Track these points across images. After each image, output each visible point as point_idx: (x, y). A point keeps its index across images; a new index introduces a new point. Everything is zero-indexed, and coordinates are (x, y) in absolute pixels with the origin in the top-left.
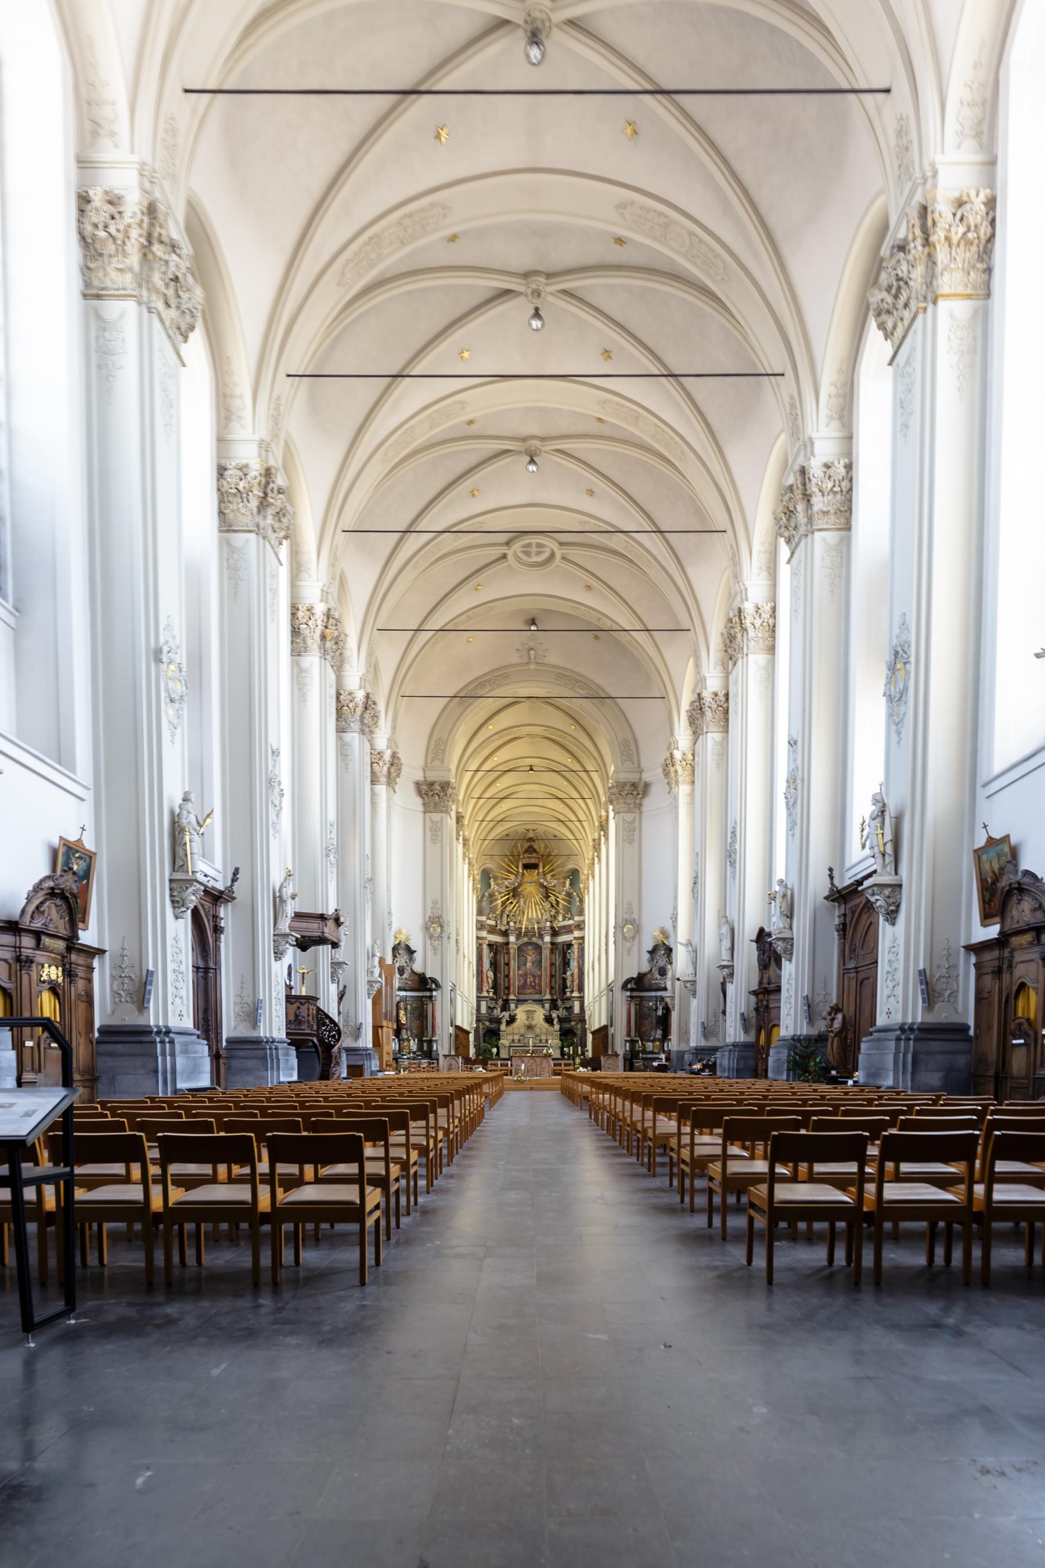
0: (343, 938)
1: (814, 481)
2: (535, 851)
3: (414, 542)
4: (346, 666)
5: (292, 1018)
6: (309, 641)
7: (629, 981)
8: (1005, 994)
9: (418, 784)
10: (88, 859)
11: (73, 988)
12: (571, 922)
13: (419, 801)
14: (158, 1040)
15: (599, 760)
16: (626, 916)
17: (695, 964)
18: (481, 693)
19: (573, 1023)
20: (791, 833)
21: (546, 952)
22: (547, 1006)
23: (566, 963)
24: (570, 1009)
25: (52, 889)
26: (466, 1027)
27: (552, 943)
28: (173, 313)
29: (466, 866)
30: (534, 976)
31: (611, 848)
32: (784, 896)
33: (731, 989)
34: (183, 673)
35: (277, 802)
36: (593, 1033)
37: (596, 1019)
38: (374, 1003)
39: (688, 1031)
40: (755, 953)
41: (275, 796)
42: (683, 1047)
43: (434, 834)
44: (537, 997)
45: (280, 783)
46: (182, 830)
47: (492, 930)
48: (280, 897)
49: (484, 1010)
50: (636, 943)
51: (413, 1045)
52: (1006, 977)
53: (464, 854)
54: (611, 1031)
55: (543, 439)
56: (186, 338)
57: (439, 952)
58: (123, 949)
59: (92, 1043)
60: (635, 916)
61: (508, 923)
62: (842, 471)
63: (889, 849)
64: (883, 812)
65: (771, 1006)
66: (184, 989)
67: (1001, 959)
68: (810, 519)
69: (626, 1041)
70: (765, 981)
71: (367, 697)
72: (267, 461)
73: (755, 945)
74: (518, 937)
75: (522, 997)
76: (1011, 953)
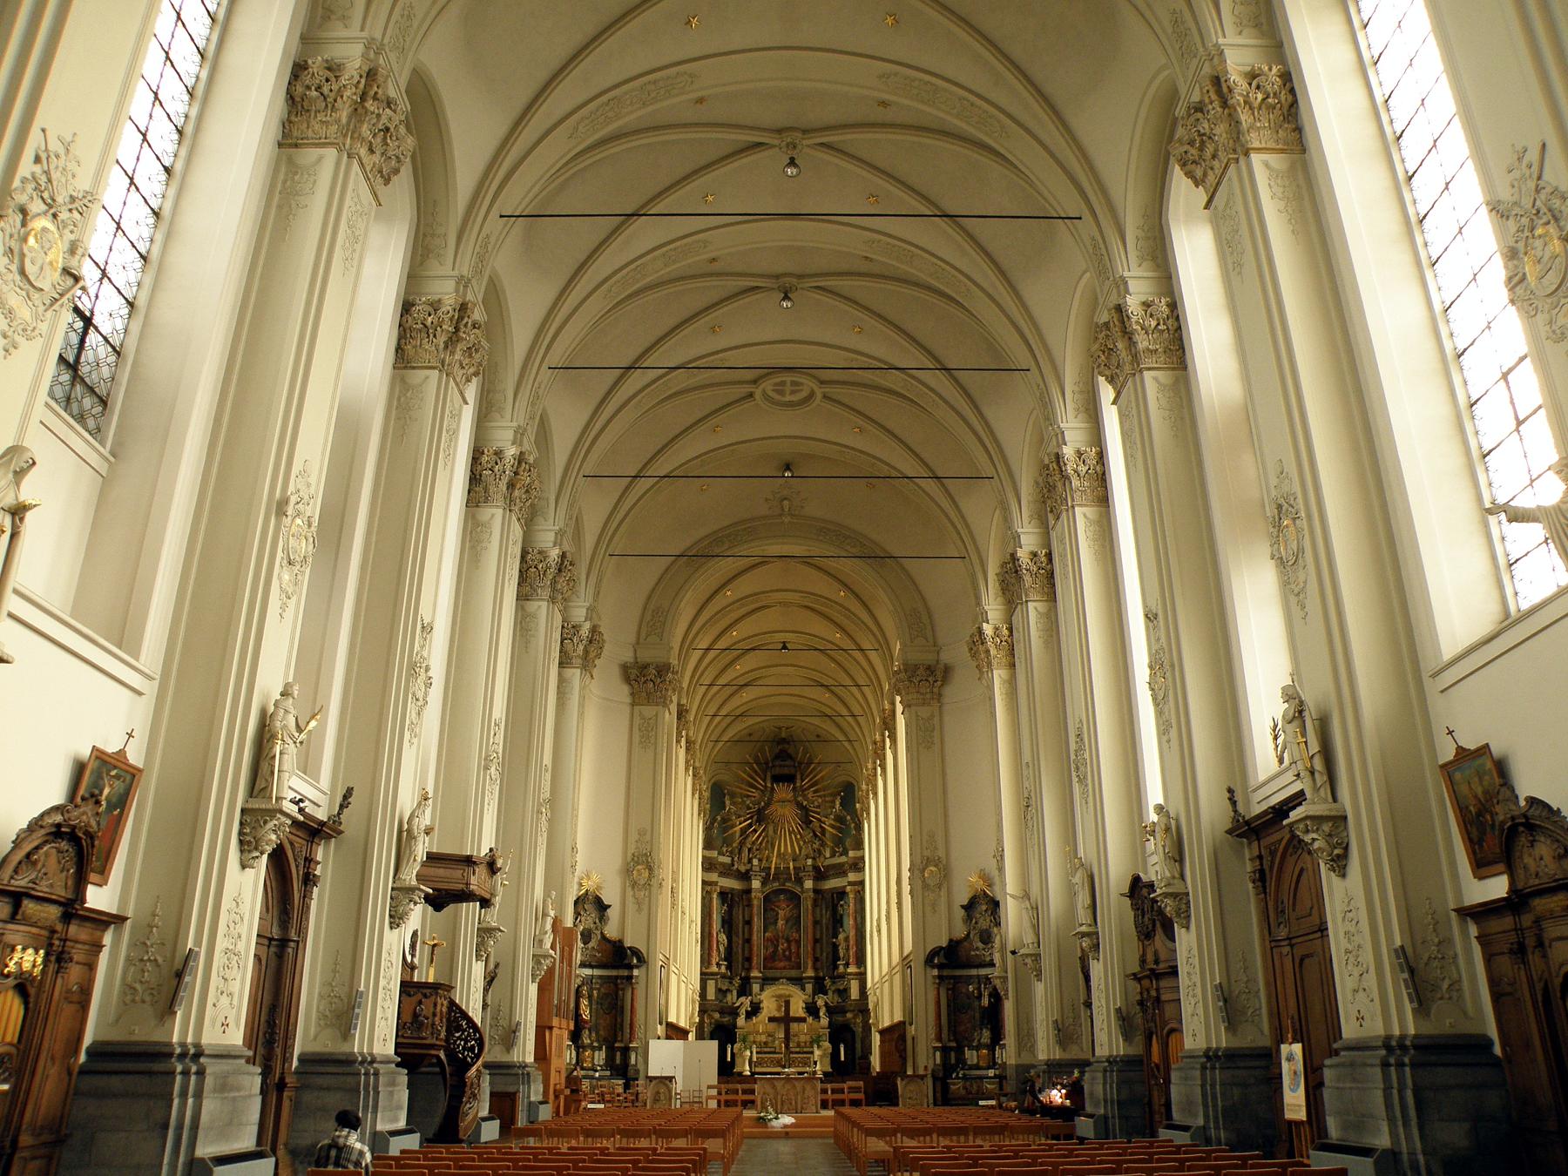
0: (500, 889)
1: (1134, 319)
2: (790, 757)
3: (637, 380)
4: (540, 520)
5: (408, 1018)
6: (492, 489)
7: (935, 952)
8: (1539, 987)
9: (625, 668)
10: (128, 778)
11: (59, 981)
12: (843, 859)
13: (626, 689)
14: (179, 1068)
15: (875, 629)
16: (927, 853)
17: (1036, 928)
18: (717, 551)
19: (849, 1015)
20: (1165, 738)
21: (807, 904)
22: (809, 987)
23: (837, 922)
24: (844, 993)
25: (59, 826)
26: (682, 1024)
27: (816, 891)
28: (376, 158)
29: (690, 780)
30: (788, 941)
31: (898, 758)
32: (1167, 829)
33: (1096, 969)
34: (313, 529)
35: (420, 695)
36: (882, 1032)
37: (887, 1012)
38: (541, 989)
39: (1034, 1030)
40: (1130, 914)
41: (418, 686)
42: (1026, 1059)
43: (643, 737)
44: (793, 973)
45: (427, 669)
46: (273, 736)
47: (726, 871)
48: (409, 831)
49: (711, 994)
50: (943, 892)
51: (600, 1057)
52: (1534, 959)
53: (687, 762)
54: (911, 1031)
55: (800, 277)
56: (387, 181)
57: (645, 907)
58: (154, 915)
59: (70, 1074)
60: (941, 853)
61: (750, 861)
62: (1165, 310)
63: (1318, 764)
64: (1301, 712)
65: (1164, 997)
66: (238, 983)
67: (1518, 930)
68: (1135, 358)
69: (936, 1049)
70: (1150, 957)
71: (563, 556)
72: (465, 294)
73: (1128, 901)
74: (764, 884)
75: (771, 973)
76: (1537, 921)
